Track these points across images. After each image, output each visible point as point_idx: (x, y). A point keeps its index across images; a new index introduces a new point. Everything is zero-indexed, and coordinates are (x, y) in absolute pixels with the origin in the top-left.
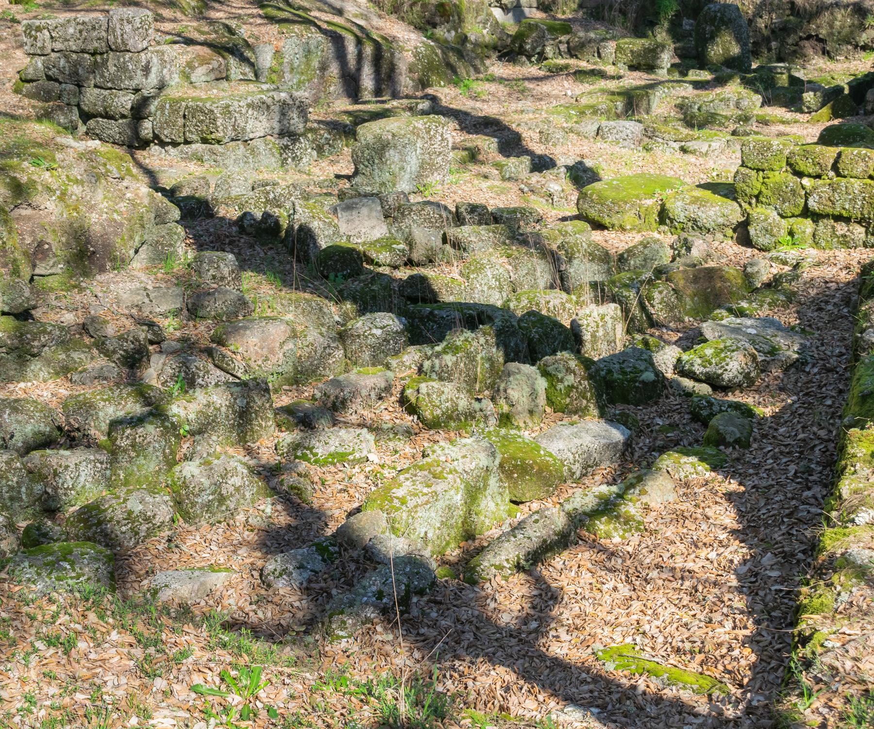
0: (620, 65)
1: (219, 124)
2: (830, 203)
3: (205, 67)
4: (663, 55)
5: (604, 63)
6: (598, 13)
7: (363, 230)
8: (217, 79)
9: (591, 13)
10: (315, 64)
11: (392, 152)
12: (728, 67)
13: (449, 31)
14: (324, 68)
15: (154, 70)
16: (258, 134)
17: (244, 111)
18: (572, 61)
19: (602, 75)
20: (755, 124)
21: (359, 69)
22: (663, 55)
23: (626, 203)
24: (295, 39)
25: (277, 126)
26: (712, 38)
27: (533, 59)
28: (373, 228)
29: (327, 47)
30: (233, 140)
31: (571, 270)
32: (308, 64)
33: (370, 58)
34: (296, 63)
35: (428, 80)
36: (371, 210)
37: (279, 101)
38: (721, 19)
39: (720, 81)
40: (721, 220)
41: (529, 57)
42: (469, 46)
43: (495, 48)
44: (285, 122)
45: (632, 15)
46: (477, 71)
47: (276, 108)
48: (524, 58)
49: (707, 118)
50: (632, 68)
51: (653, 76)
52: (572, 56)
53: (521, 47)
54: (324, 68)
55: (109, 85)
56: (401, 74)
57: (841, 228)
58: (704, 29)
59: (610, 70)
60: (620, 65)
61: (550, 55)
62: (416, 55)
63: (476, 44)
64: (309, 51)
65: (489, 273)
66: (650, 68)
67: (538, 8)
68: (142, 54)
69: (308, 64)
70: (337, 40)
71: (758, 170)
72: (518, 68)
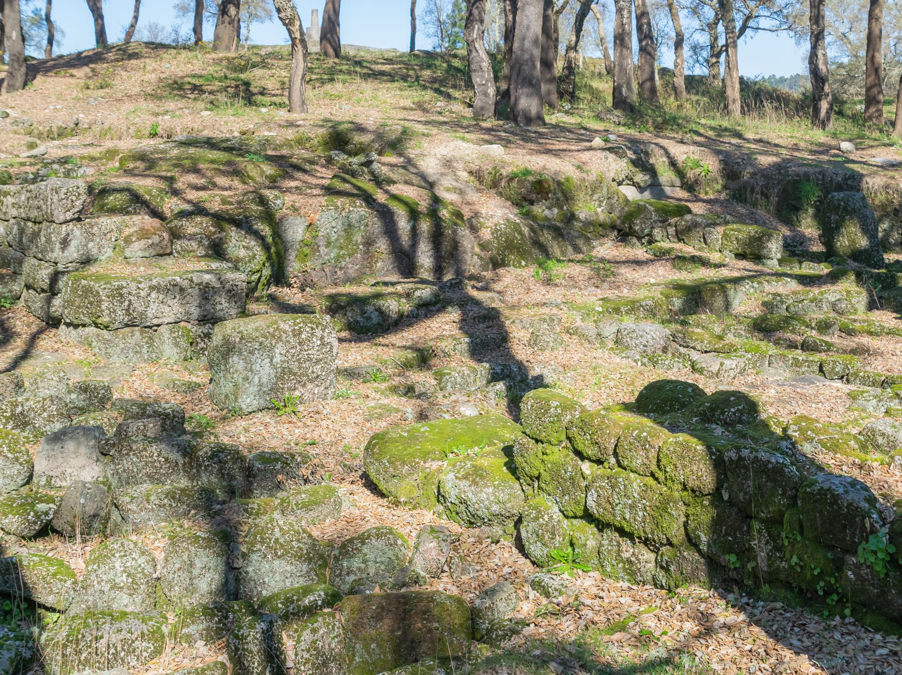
0: (726, 253)
1: (103, 307)
2: (608, 507)
3: (143, 242)
4: (769, 245)
5: (711, 250)
6: (740, 195)
7: (69, 471)
8: (161, 255)
9: (734, 195)
10: (358, 238)
11: (235, 358)
12: (855, 260)
13: (549, 208)
14: (369, 243)
15: (74, 244)
16: (166, 320)
17: (143, 294)
18: (678, 246)
19: (704, 263)
20: (837, 333)
21: (414, 245)
22: (769, 245)
23: (404, 463)
24: (333, 212)
25: (195, 312)
26: (838, 228)
27: (643, 241)
28: (83, 467)
29: (375, 225)
30: (127, 325)
31: (250, 569)
32: (349, 238)
33: (426, 234)
34: (334, 237)
35: (503, 260)
36: (79, 444)
37: (199, 284)
38: (845, 209)
39: (834, 278)
40: (495, 508)
41: (639, 238)
42: (577, 225)
43: (613, 227)
44: (208, 307)
45: (774, 199)
46: (577, 249)
47: (196, 292)
48: (635, 240)
49: (779, 323)
50: (740, 256)
51: (759, 268)
52: (680, 240)
53: (630, 228)
54: (369, 243)
55: (40, 256)
56: (465, 252)
57: (628, 550)
58: (829, 217)
59: (715, 257)
60: (726, 253)
61: (658, 238)
62: (495, 232)
63: (588, 224)
64: (349, 225)
65: (118, 565)
66: (758, 258)
67: (681, 187)
68: (64, 226)
69: (349, 238)
70: (386, 215)
71: (537, 441)
72: (628, 249)
